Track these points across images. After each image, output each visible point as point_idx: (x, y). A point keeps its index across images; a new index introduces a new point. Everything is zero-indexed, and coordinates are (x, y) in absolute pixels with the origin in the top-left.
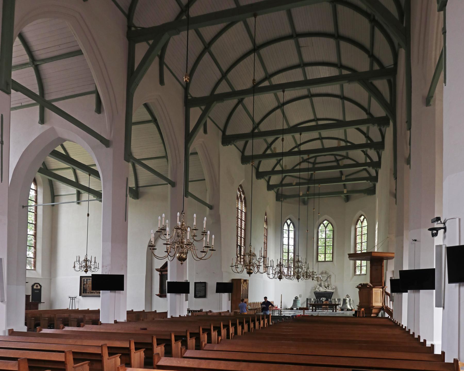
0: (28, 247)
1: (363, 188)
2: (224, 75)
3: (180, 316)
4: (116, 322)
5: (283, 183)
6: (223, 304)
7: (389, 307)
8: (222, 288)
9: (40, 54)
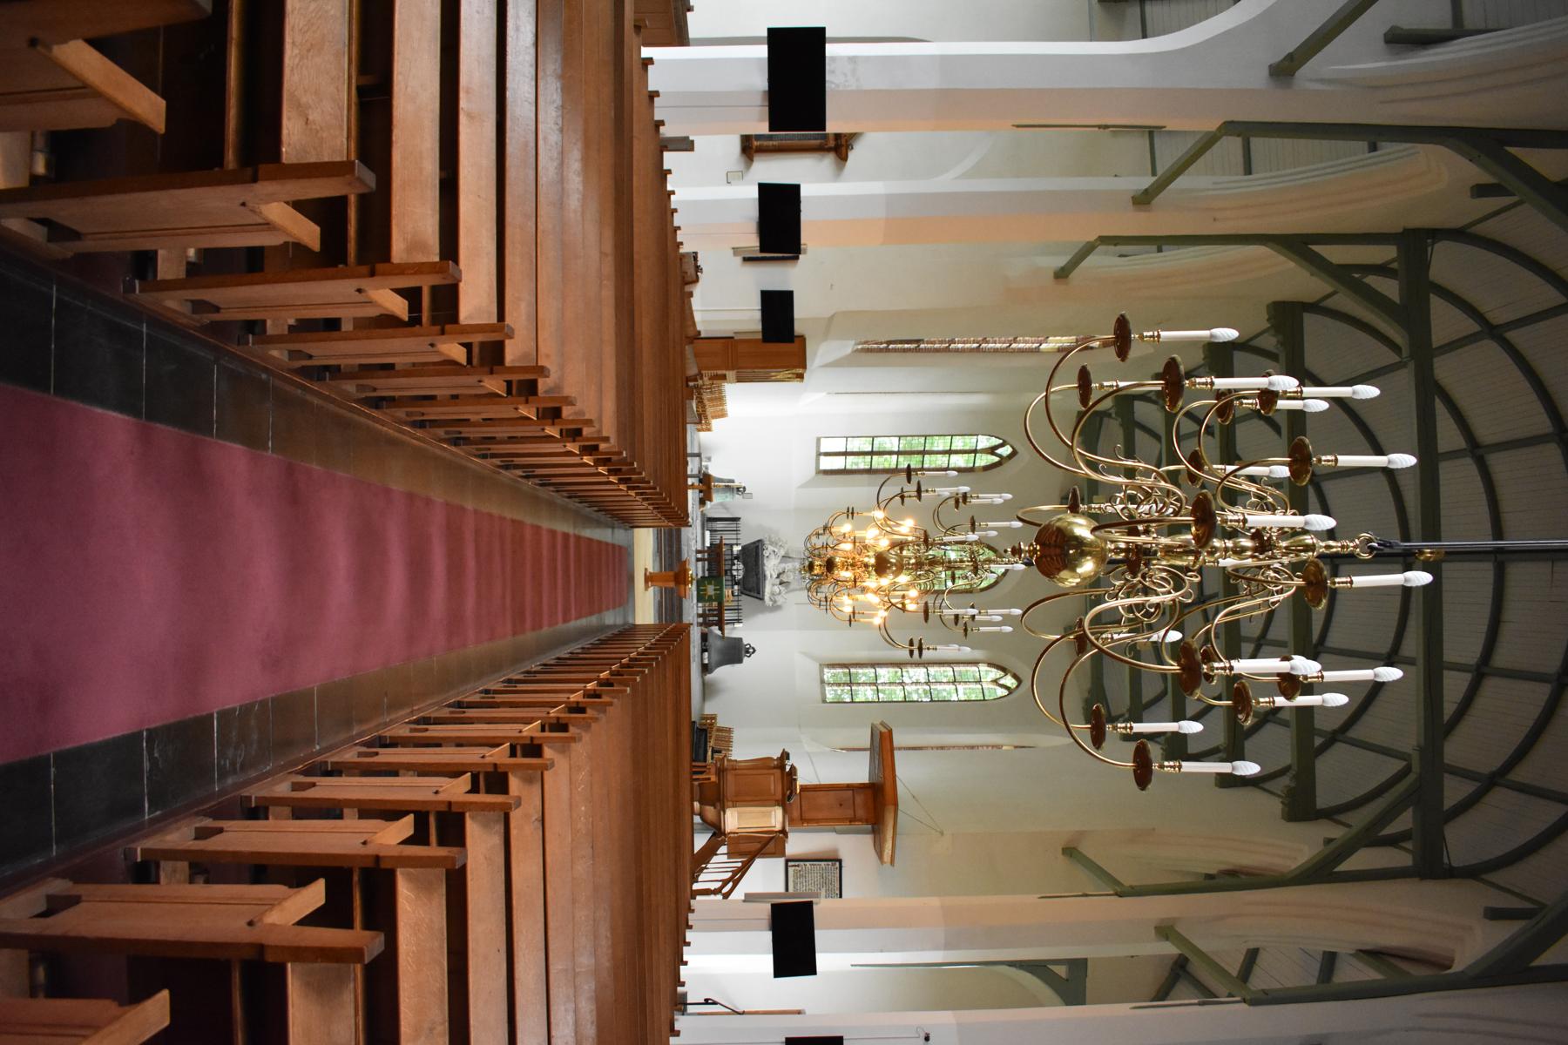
1: (1109, 684)
2: (1493, 331)
3: (669, 171)
4: (654, 95)
5: (1138, 434)
6: (725, 300)
8: (777, 306)
9: (1486, 433)
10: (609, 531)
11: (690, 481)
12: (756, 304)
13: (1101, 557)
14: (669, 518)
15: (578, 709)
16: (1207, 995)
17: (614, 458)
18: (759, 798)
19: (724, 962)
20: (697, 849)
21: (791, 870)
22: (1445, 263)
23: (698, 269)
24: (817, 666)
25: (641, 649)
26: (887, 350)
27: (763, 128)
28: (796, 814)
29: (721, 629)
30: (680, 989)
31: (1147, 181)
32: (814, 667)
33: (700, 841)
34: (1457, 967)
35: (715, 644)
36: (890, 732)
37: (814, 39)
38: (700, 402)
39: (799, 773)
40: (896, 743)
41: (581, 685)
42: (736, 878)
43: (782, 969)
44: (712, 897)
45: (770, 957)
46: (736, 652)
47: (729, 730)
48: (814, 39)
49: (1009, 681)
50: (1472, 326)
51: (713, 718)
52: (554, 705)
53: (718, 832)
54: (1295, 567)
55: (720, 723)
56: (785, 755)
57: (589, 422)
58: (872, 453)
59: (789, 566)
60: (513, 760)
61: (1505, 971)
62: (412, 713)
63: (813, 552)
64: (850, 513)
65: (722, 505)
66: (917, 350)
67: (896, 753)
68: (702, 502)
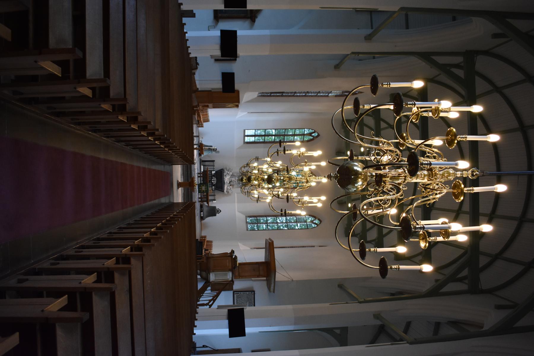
0: (286, 152)
6: (208, 77)
8: (228, 79)
10: (163, 166)
11: (195, 147)
12: (220, 78)
13: (364, 180)
14: (186, 161)
15: (147, 240)
16: (394, 339)
17: (162, 137)
18: (224, 269)
19: (211, 331)
21: (235, 295)
22: (482, 64)
23: (197, 64)
24: (245, 217)
25: (175, 213)
26: (270, 96)
27: (221, 7)
28: (237, 274)
29: (208, 203)
31: (369, 31)
33: (200, 285)
34: (485, 328)
35: (205, 209)
36: (273, 242)
38: (199, 116)
39: (238, 258)
41: (149, 230)
42: (214, 299)
43: (232, 334)
44: (205, 307)
45: (228, 330)
46: (213, 212)
47: (211, 242)
49: (317, 221)
50: (490, 88)
51: (205, 237)
52: (137, 239)
53: (207, 283)
54: (445, 183)
55: (208, 239)
56: (233, 252)
57: (149, 123)
58: (265, 136)
59: (233, 179)
60: (131, 253)
61: (503, 329)
62: (77, 244)
63: (243, 174)
64: (257, 159)
65: (207, 155)
66: (282, 96)
67: (275, 249)
68: (200, 155)
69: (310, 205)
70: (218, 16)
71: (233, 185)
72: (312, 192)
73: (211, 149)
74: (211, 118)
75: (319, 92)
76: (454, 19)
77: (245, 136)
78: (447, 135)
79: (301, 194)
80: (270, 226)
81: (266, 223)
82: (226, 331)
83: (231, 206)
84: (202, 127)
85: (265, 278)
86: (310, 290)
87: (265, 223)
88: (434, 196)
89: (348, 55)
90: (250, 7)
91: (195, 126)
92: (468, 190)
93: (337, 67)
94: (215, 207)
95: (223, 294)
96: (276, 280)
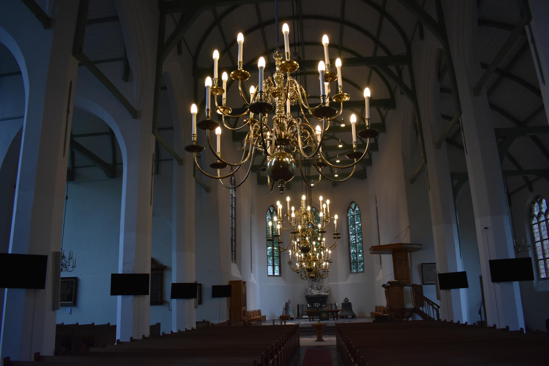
6: (216, 311)
7: (432, 316)
8: (219, 291)
11: (283, 324)
12: (217, 300)
13: (284, 156)
16: (459, 130)
20: (422, 319)
21: (427, 282)
23: (204, 321)
25: (344, 343)
26: (235, 251)
27: (148, 298)
29: (339, 311)
30: (477, 324)
31: (175, 161)
32: (351, 276)
33: (419, 318)
35: (345, 313)
36: (373, 247)
37: (115, 278)
38: (254, 320)
40: (377, 244)
42: (432, 304)
43: (465, 285)
44: (440, 312)
45: (460, 289)
46: (347, 305)
47: (376, 307)
48: (115, 278)
49: (353, 206)
51: (372, 313)
53: (415, 310)
55: (374, 310)
56: (384, 286)
58: (273, 256)
59: (315, 286)
66: (235, 240)
67: (381, 244)
68: (292, 319)
69: (328, 211)
70: (158, 300)
71: (321, 287)
72: (316, 210)
73: (287, 308)
74: (257, 308)
75: (232, 206)
76: (165, 88)
77: (274, 275)
78: (238, 79)
79: (318, 219)
80: (359, 250)
81: (356, 254)
82: (462, 291)
83: (342, 288)
84: (265, 316)
85: (409, 254)
86: (417, 209)
87: (357, 255)
88: (298, 90)
89: (196, 180)
90: (148, 271)
91: (263, 324)
92: (288, 58)
93: (208, 190)
94: (342, 304)
95: (426, 295)
96: (410, 243)
